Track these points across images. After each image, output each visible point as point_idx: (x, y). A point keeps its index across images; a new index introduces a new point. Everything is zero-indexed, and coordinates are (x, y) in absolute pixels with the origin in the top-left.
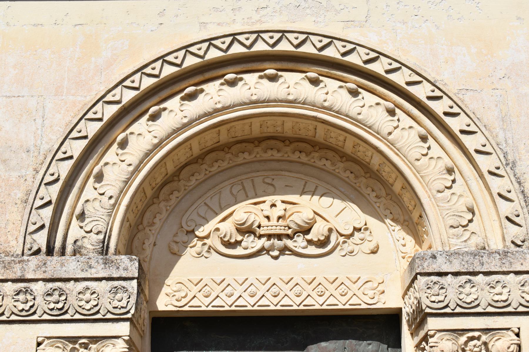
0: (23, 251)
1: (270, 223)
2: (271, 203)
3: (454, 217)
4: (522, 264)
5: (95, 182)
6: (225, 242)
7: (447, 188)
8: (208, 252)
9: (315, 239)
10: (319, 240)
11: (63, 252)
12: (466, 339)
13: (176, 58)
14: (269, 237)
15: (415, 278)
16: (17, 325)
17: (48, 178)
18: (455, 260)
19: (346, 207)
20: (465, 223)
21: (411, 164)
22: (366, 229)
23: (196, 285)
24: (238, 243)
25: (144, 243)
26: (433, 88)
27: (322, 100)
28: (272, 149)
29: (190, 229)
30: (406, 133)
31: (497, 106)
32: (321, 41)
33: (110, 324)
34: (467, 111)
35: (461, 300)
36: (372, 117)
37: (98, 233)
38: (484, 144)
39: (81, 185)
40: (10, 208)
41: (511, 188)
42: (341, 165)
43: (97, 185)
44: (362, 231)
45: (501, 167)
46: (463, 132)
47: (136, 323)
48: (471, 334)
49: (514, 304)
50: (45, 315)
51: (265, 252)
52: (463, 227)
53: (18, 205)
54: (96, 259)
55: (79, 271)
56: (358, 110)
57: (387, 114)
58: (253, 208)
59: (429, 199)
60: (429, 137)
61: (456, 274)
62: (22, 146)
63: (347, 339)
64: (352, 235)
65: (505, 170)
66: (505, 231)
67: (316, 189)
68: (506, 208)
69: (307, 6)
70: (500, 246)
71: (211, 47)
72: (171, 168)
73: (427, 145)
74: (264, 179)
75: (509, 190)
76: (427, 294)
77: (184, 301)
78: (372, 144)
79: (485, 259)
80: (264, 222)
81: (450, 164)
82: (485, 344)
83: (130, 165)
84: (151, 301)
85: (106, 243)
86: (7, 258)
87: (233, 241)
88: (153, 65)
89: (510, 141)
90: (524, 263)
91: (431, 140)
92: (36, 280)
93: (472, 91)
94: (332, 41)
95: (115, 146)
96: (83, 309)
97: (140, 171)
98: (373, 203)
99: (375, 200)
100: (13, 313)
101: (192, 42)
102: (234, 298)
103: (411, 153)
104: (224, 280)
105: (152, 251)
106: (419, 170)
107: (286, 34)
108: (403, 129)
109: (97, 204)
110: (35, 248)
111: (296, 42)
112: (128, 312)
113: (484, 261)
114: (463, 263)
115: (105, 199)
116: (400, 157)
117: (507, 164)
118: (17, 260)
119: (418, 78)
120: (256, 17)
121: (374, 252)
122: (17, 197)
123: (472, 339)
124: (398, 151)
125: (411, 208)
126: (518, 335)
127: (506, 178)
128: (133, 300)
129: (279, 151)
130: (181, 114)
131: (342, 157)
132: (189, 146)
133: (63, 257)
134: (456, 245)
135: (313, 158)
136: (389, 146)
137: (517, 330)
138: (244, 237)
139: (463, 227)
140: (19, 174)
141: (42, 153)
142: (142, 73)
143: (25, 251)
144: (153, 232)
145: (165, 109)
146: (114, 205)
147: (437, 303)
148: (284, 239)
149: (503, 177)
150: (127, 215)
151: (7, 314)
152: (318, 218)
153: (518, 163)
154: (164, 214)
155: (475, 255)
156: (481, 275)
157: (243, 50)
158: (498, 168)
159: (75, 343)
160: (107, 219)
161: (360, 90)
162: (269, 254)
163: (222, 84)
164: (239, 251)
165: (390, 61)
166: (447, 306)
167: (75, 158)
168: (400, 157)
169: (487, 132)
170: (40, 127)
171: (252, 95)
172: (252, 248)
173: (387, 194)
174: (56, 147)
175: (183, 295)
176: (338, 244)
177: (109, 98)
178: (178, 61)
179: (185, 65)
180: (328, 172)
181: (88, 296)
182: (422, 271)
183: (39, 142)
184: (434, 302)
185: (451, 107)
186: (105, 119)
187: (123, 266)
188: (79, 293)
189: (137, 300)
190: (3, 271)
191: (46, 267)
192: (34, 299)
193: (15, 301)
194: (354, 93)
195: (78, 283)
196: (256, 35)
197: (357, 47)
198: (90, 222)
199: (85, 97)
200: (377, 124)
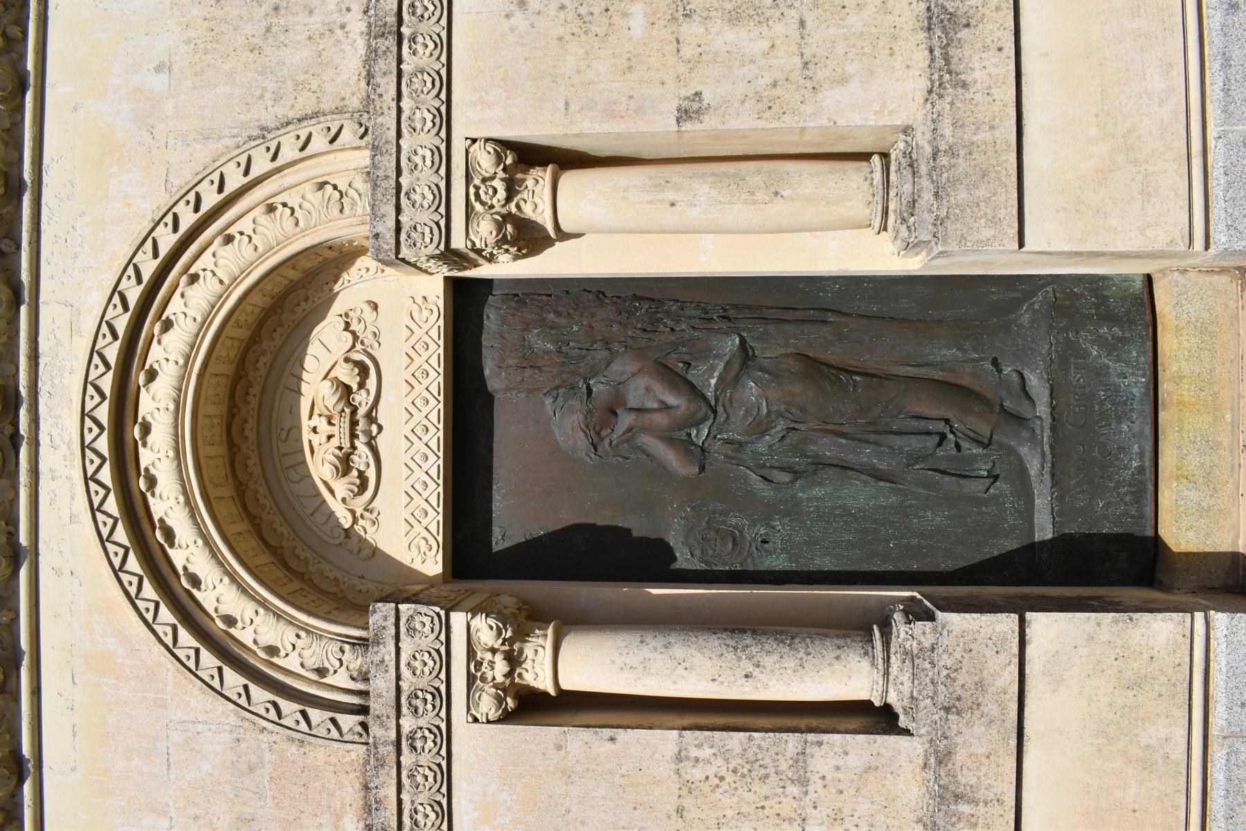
0: (362, 743)
1: (337, 434)
2: (312, 433)
3: (330, 207)
4: (388, 129)
5: (278, 656)
6: (359, 491)
7: (293, 213)
8: (371, 512)
9: (358, 379)
10: (359, 374)
11: (364, 694)
12: (478, 203)
13: (116, 554)
15: (403, 260)
16: (453, 748)
17: (273, 715)
18: (381, 210)
19: (1021, 245)
20: (337, 195)
21: (261, 257)
22: (347, 315)
23: (413, 527)
24: (361, 475)
25: (360, 591)
26: (162, 224)
27: (176, 366)
28: (243, 430)
29: (343, 534)
30: (221, 262)
31: (188, 145)
32: (97, 366)
33: (452, 636)
34: (194, 183)
35: (430, 206)
36: (199, 304)
37: (342, 651)
38: (237, 165)
39: (282, 673)
40: (309, 761)
41: (293, 134)
42: (265, 344)
43: (283, 653)
44: (349, 320)
45: (267, 144)
46: (220, 190)
47: (454, 603)
48: (472, 197)
49: (437, 142)
50: (440, 715)
51: (373, 441)
52: (342, 197)
53: (307, 751)
54: (374, 655)
55: (387, 675)
56: (189, 321)
57: (196, 284)
58: (319, 455)
59: (307, 238)
60: (227, 232)
62: (232, 749)
63: (481, 344)
64: (354, 333)
65: (271, 140)
66: (347, 146)
67: (296, 376)
68: (318, 144)
69: (50, 383)
70: (367, 153)
71: (102, 509)
72: (265, 559)
73: (238, 236)
74: (281, 441)
75: (295, 138)
76: (422, 248)
77: (432, 541)
78: (235, 304)
79: (381, 173)
80: (335, 442)
81: (262, 208)
82: (484, 180)
83: (257, 612)
84: (431, 582)
85: (355, 641)
86: (372, 763)
87: (358, 481)
88: (126, 584)
89: (235, 131)
90: (387, 126)
91: (231, 231)
92: (398, 727)
93: (169, 175)
94: (97, 352)
95: (232, 631)
96: (433, 669)
97: (265, 600)
98: (315, 305)
99: (310, 302)
100: (438, 753)
101: (95, 533)
102: (429, 481)
103: (247, 257)
104: (406, 492)
105: (370, 580)
106: (268, 248)
107: (86, 412)
108: (216, 265)
109: (306, 653)
110: (359, 729)
111: (97, 399)
112: (438, 614)
113: (384, 174)
114: (385, 200)
115: (299, 643)
116: (252, 270)
117: (264, 137)
118: (373, 751)
119: (149, 243)
120: (64, 450)
121: (375, 307)
122: (297, 752)
123: (477, 196)
125: (320, 259)
126: (474, 141)
127: (281, 139)
128: (423, 609)
129: (246, 421)
130: (192, 548)
131: (255, 342)
132: (236, 536)
133: (371, 694)
134: (364, 207)
135: (256, 378)
136: (238, 284)
137: (469, 142)
138: (353, 467)
139: (342, 197)
140: (267, 751)
141: (240, 724)
142: (136, 598)
143: (363, 741)
144: (346, 579)
145: (185, 568)
146: (308, 632)
147: (433, 235)
148: (357, 418)
149: (279, 143)
150: (322, 614)
151: (439, 760)
152: (332, 375)
153: (263, 123)
154: (325, 566)
155: (376, 185)
156: (400, 179)
157: (107, 467)
158: (268, 149)
159: (475, 677)
160: (325, 641)
161: (164, 318)
162: (376, 437)
163: (153, 495)
164: (371, 474)
165: (125, 278)
166: (437, 224)
167: (246, 682)
168: (252, 270)
169: (221, 159)
170: (208, 727)
171: (168, 457)
172: (367, 457)
173: (304, 287)
174: (232, 706)
175: (424, 542)
176: (365, 351)
177: (169, 640)
178: (121, 552)
179: (127, 543)
180: (274, 360)
181: (417, 664)
182: (394, 251)
183: (226, 727)
184: (432, 239)
185: (188, 202)
186: (197, 645)
187: (381, 622)
188: (415, 674)
189: (423, 604)
190: (387, 767)
191: (383, 715)
192: (421, 728)
193: (423, 751)
194: (168, 325)
195: (402, 676)
196: (87, 451)
197: (106, 319)
198: (329, 661)
199: (168, 670)
200: (209, 297)
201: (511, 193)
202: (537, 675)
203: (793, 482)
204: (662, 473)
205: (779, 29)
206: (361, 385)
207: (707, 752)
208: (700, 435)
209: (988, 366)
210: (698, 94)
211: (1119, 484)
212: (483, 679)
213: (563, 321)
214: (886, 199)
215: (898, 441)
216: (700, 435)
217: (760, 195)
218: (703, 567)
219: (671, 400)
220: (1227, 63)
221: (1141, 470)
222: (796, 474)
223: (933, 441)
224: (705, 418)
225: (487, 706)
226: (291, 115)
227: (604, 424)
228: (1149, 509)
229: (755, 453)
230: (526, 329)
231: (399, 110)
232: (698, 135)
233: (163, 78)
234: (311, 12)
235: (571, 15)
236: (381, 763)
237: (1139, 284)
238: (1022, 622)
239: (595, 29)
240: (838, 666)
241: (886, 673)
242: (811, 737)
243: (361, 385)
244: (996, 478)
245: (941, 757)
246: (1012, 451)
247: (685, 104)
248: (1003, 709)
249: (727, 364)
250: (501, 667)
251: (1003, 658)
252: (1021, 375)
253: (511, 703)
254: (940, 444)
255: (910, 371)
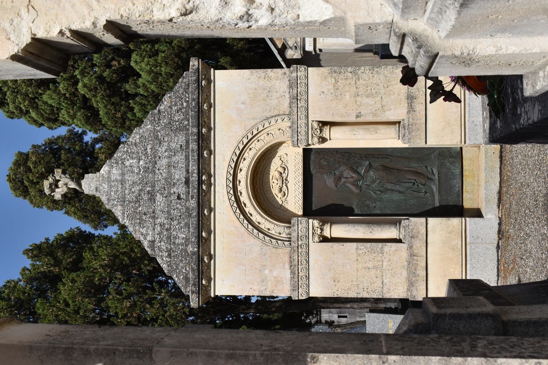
14: (283, 184)
17: (270, 242)
21: (266, 145)
24: (284, 192)
30: (257, 146)
49: (306, 122)
56: (250, 159)
61: (298, 136)
77: (300, 207)
80: (279, 185)
109: (276, 230)
121: (287, 155)
123: (314, 133)
124: (262, 148)
130: (250, 208)
164: (286, 192)
181: (302, 230)
201: (321, 132)
202: (327, 233)
203: (381, 193)
204: (351, 192)
205: (377, 99)
206: (284, 172)
207: (363, 247)
208: (360, 183)
209: (424, 167)
210: (360, 112)
211: (454, 194)
212: (316, 233)
213: (329, 158)
214: (399, 134)
215: (404, 184)
216: (360, 183)
217: (373, 133)
218: (361, 213)
219: (354, 175)
220: (469, 106)
221: (459, 190)
222: (382, 192)
223: (412, 184)
224: (361, 179)
225: (316, 239)
226: (273, 115)
227: (338, 181)
228: (461, 199)
229: (372, 187)
230: (321, 159)
231: (298, 115)
232: (359, 120)
233: (244, 105)
234: (277, 92)
235: (334, 95)
236: (294, 251)
237: (459, 149)
238: (427, 220)
239: (339, 98)
240: (390, 230)
241: (400, 231)
242: (384, 244)
243: (284, 172)
244: (426, 193)
245: (411, 247)
246: (430, 187)
247: (357, 114)
248: (423, 237)
249: (366, 168)
250: (319, 231)
251: (423, 227)
252: (432, 170)
253: (321, 238)
254: (413, 185)
255: (407, 169)
